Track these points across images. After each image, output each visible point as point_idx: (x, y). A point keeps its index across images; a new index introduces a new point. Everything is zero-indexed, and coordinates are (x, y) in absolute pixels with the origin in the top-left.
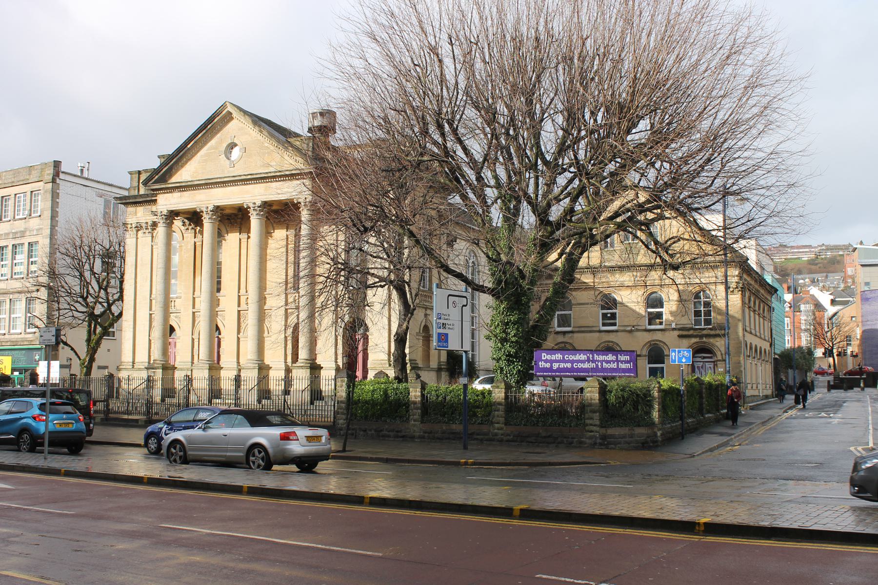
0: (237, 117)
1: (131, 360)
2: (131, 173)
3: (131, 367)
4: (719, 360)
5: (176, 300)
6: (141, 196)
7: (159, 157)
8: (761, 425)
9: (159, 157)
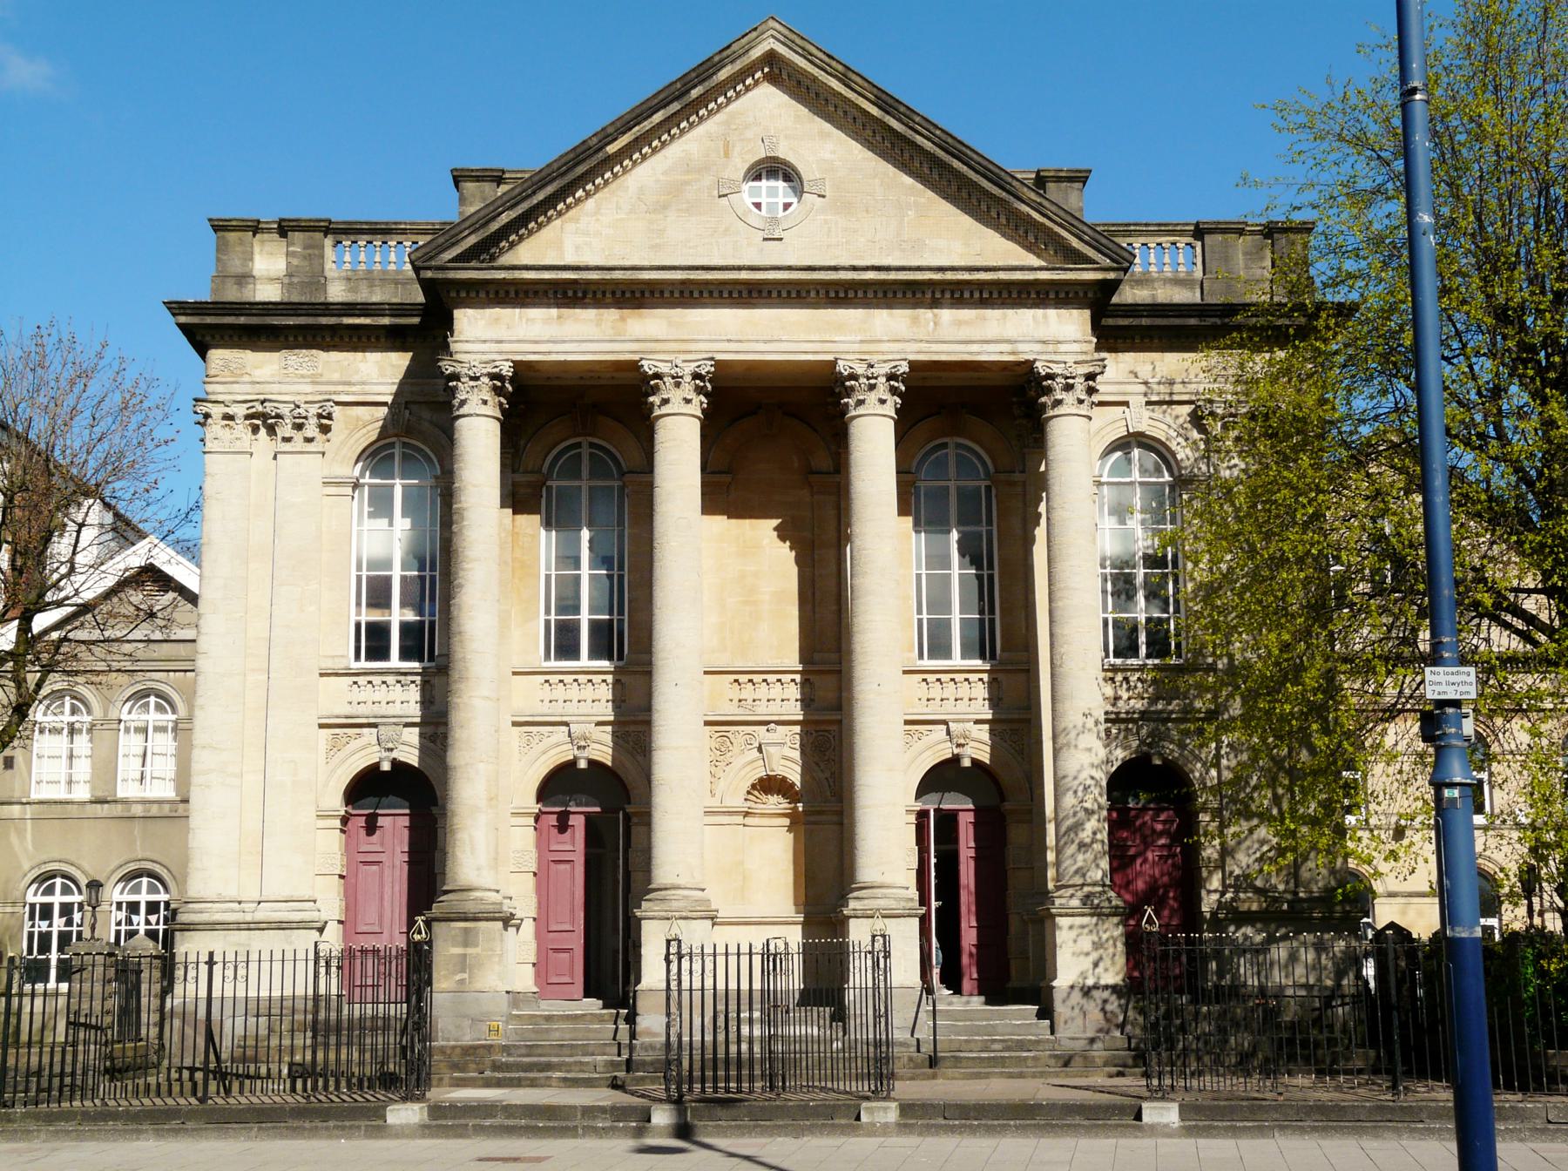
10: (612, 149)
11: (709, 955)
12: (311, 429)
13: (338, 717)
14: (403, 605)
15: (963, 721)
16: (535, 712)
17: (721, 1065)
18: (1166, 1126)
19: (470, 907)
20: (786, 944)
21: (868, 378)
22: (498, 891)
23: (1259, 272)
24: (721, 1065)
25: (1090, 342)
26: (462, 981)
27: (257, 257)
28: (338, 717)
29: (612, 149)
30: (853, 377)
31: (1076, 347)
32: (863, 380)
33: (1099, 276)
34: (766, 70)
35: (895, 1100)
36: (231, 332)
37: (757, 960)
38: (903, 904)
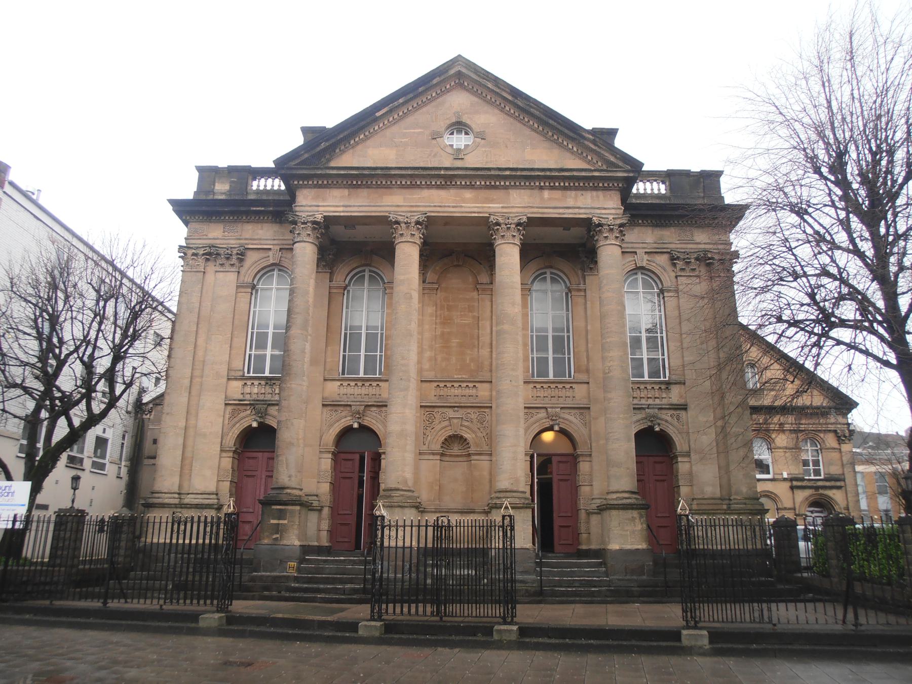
10: (378, 114)
11: (415, 526)
12: (234, 260)
13: (235, 400)
14: (273, 347)
15: (555, 408)
16: (334, 400)
17: (462, 566)
18: (701, 647)
19: (285, 498)
20: (449, 521)
21: (506, 225)
22: (301, 490)
23: (697, 194)
24: (462, 566)
25: (621, 209)
26: (276, 539)
27: (217, 184)
28: (235, 400)
29: (378, 114)
30: (498, 224)
31: (613, 211)
32: (503, 226)
33: (625, 175)
34: (457, 81)
35: (516, 624)
37: (430, 530)
38: (523, 501)
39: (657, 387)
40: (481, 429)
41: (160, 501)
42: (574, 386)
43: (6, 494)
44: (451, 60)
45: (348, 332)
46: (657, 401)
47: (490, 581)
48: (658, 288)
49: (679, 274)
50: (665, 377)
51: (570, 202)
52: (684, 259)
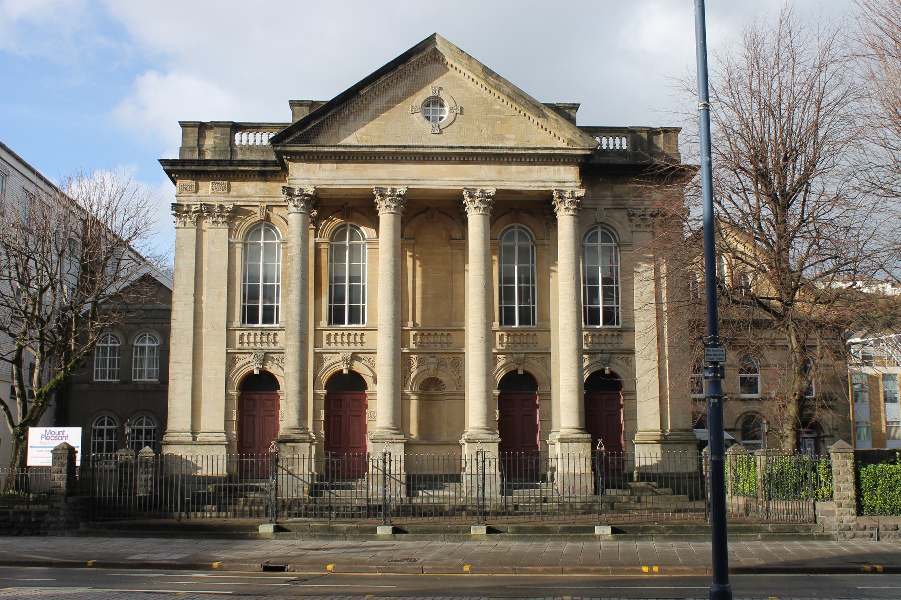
0: (455, 65)
1: (189, 428)
2: (184, 125)
3: (191, 439)
4: (827, 436)
5: (277, 332)
6: (207, 163)
7: (293, 104)
8: (479, 539)
9: (293, 104)
36: (188, 174)
39: (610, 334)
40: (455, 373)
41: (176, 439)
42: (537, 333)
43: (60, 438)
44: (428, 39)
45: (333, 285)
46: (610, 347)
47: (465, 500)
48: (615, 241)
49: (635, 229)
50: (618, 324)
51: (535, 176)
52: (640, 216)
